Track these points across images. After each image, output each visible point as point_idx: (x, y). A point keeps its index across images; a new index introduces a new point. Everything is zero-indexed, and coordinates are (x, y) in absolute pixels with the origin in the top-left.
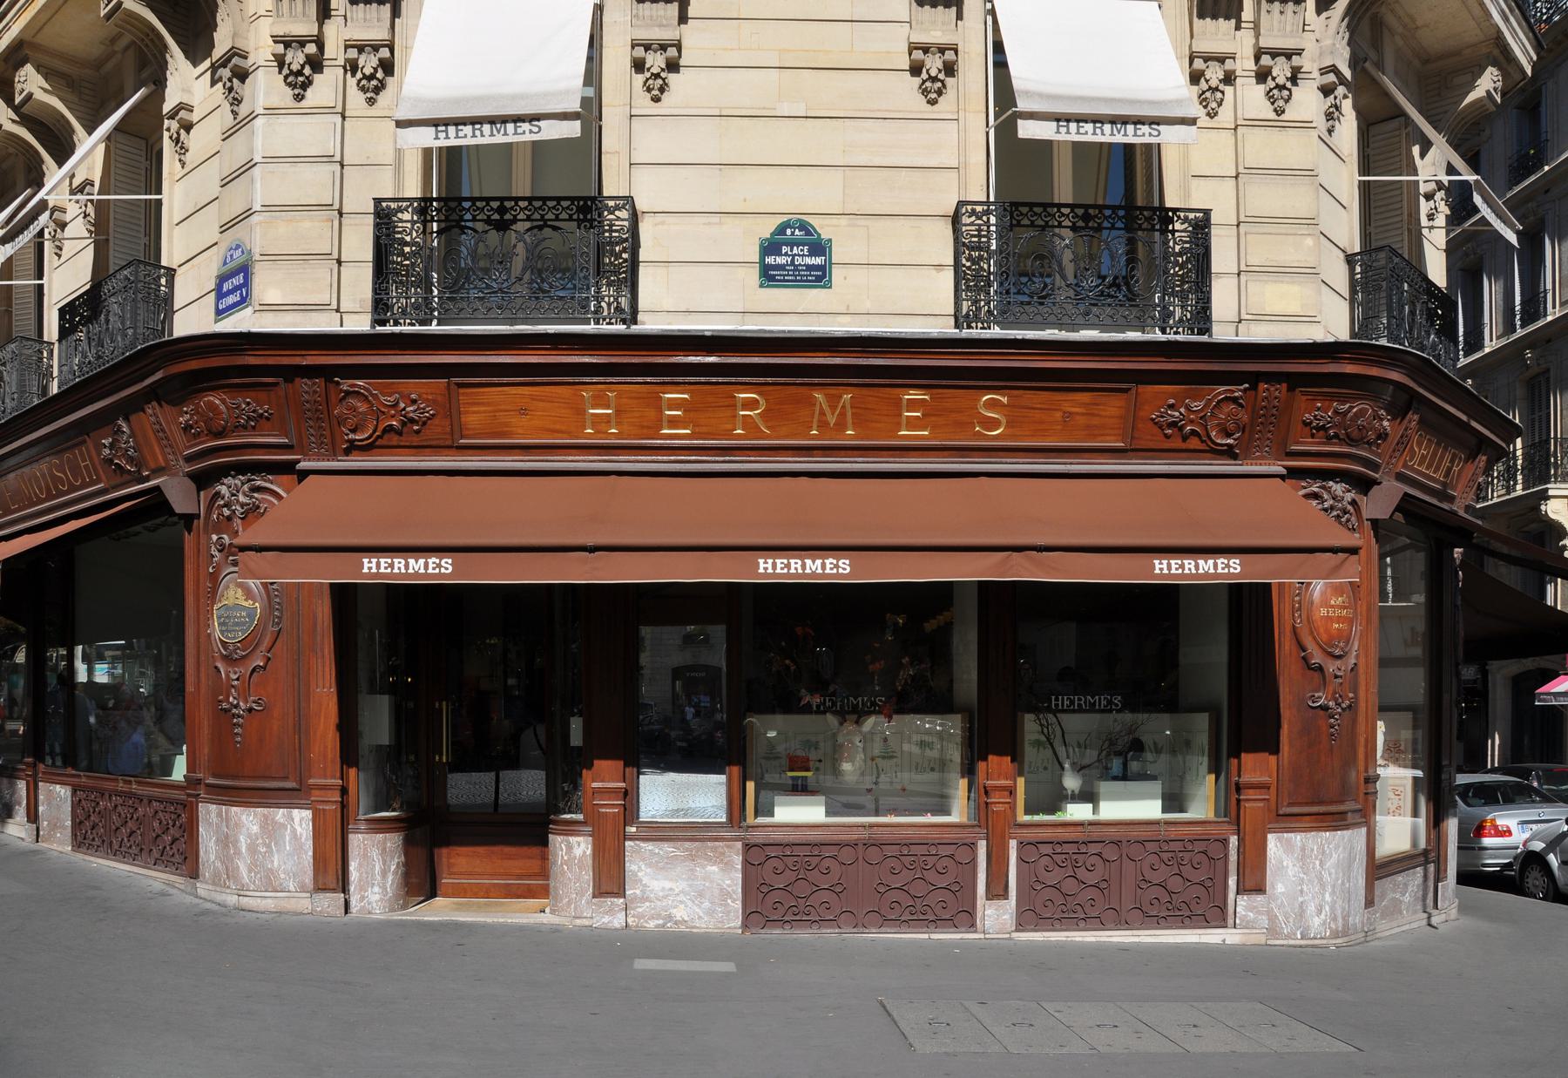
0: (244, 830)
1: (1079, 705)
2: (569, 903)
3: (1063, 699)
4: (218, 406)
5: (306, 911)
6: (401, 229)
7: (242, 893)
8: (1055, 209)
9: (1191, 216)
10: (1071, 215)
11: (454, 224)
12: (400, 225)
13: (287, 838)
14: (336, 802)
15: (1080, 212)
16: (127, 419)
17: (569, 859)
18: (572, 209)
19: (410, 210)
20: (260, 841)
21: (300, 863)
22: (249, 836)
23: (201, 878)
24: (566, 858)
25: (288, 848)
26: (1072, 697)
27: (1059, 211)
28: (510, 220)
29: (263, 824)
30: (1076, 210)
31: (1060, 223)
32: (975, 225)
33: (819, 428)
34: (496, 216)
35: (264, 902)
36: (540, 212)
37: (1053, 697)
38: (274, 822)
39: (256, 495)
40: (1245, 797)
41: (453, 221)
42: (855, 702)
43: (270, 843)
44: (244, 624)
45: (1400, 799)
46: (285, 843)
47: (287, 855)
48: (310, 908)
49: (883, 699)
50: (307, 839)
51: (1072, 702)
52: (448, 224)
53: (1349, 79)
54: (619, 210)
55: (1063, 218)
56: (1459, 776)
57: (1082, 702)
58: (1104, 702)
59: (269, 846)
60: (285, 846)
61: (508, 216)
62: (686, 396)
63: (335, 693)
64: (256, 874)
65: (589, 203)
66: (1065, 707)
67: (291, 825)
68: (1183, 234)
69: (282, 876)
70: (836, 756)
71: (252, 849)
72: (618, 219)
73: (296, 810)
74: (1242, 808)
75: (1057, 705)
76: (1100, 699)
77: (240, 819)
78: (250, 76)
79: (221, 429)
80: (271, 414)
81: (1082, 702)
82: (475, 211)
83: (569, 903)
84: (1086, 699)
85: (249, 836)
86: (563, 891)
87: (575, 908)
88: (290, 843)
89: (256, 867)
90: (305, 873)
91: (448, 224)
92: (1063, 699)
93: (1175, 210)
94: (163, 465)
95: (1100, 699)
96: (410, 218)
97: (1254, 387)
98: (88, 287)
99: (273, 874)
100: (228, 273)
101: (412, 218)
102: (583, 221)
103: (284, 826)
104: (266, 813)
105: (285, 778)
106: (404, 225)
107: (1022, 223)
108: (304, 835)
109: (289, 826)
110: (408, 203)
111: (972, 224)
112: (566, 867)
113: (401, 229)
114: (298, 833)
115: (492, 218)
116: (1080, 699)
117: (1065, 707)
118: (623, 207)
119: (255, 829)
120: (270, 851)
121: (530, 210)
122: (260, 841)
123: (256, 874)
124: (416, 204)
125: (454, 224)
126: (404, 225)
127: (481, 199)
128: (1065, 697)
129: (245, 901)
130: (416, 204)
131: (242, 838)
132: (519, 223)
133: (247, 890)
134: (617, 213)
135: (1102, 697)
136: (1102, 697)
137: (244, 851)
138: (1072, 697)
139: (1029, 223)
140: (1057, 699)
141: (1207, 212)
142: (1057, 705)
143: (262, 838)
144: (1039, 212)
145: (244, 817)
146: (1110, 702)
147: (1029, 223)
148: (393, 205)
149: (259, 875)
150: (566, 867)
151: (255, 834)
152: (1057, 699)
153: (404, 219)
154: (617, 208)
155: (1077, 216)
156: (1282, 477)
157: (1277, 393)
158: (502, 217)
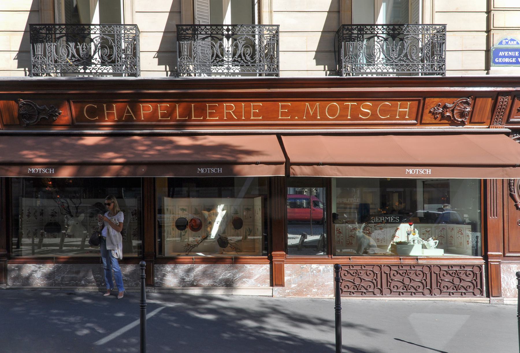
6: (41, 37)
8: (375, 27)
9: (438, 27)
10: (387, 29)
11: (64, 35)
12: (41, 35)
15: (391, 27)
18: (95, 30)
19: (191, 29)
27: (377, 27)
28: (396, 34)
30: (390, 27)
31: (366, 32)
32: (349, 34)
33: (399, 116)
34: (391, 32)
36: (88, 30)
40: (275, 260)
41: (63, 33)
45: (429, 234)
49: (398, 217)
51: (379, 219)
52: (61, 35)
54: (188, 30)
55: (218, 31)
58: (392, 219)
61: (396, 32)
62: (390, 104)
65: (362, 27)
66: (391, 221)
68: (347, 35)
70: (196, 243)
72: (187, 34)
74: (274, 264)
76: (390, 218)
82: (61, 30)
84: (385, 218)
91: (61, 35)
93: (200, 26)
95: (390, 218)
96: (357, 33)
97: (475, 99)
101: (358, 32)
102: (48, 34)
106: (43, 35)
107: (368, 33)
110: (44, 26)
111: (347, 34)
113: (41, 37)
115: (390, 32)
117: (391, 221)
118: (190, 29)
121: (399, 30)
124: (359, 27)
125: (64, 35)
126: (43, 35)
127: (397, 25)
130: (359, 27)
132: (401, 35)
134: (187, 31)
135: (391, 217)
136: (391, 217)
139: (370, 33)
141: (444, 26)
144: (380, 28)
146: (395, 219)
147: (370, 33)
148: (38, 27)
153: (189, 33)
154: (187, 29)
155: (390, 29)
156: (508, 134)
157: (506, 100)
158: (228, 33)
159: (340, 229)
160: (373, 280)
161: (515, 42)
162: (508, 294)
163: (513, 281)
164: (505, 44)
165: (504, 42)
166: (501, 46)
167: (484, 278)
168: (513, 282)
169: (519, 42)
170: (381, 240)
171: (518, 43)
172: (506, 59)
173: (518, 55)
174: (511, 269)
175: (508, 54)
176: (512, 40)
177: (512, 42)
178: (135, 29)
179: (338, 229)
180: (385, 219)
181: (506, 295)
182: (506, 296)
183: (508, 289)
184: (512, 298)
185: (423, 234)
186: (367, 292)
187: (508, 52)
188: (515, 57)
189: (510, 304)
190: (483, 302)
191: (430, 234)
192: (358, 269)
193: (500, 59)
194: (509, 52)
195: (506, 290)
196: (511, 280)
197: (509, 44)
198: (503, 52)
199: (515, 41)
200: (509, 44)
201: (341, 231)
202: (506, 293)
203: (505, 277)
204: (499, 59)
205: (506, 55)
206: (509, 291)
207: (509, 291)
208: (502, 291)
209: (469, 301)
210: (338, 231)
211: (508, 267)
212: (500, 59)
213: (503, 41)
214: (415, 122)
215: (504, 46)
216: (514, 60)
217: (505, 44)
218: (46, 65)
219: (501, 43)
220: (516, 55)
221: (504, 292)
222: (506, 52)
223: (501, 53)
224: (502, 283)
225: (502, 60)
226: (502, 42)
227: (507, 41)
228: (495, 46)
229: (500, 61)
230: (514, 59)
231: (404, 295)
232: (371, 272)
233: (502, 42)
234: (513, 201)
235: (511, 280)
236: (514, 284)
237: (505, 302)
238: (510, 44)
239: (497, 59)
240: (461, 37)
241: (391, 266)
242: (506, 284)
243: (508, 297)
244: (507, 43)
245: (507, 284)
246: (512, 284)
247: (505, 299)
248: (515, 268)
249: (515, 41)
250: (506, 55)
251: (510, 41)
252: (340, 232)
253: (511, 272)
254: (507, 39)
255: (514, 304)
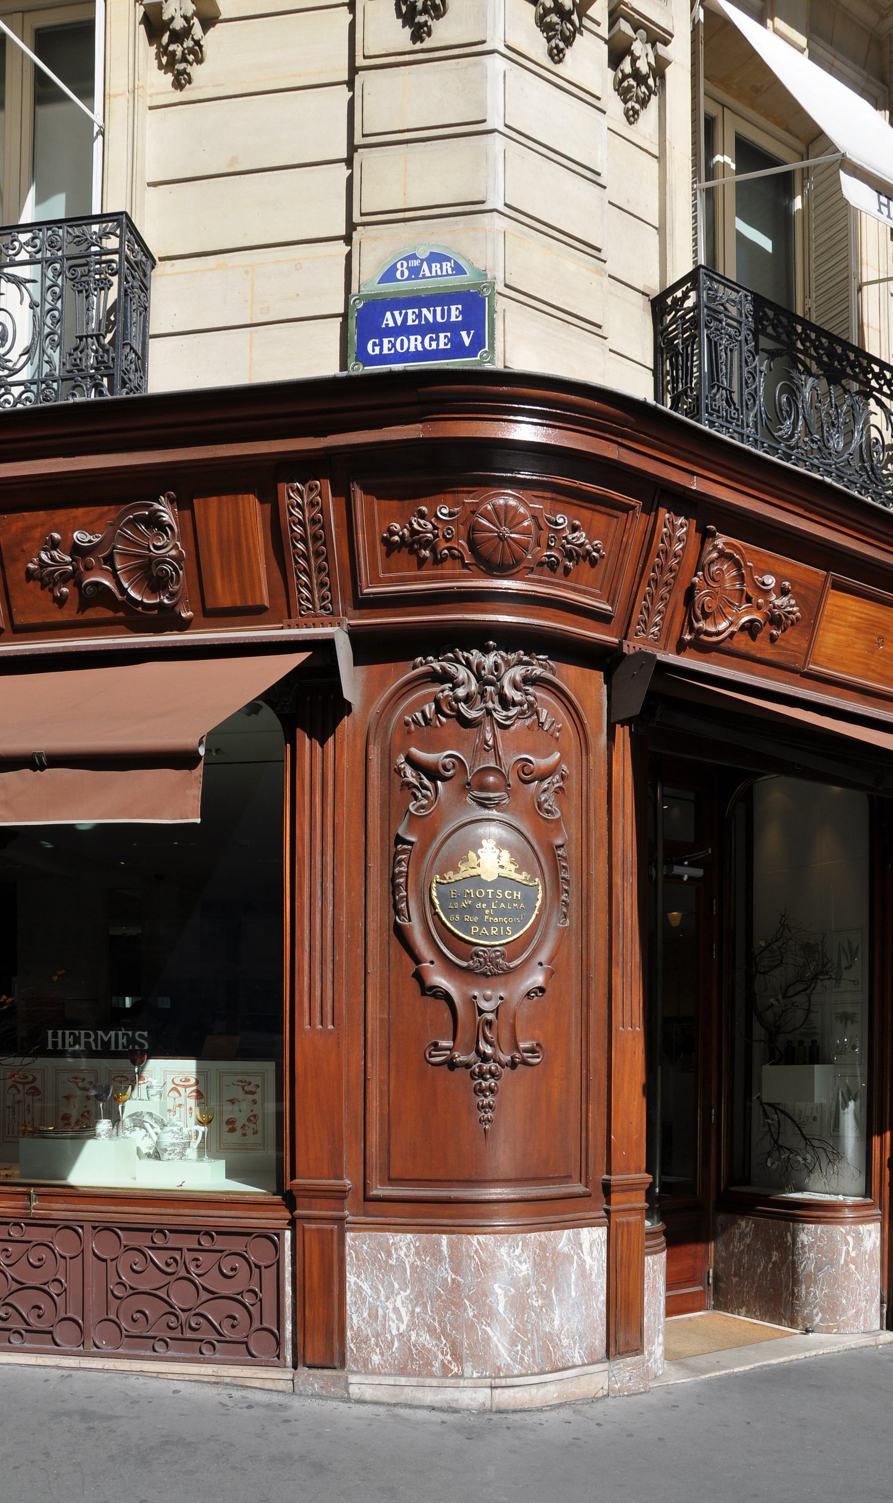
0: (503, 1274)
1: (88, 1044)
2: (858, 1315)
3: (63, 1034)
4: (515, 508)
5: (600, 1394)
7: (498, 1382)
13: (573, 1277)
14: (641, 1209)
16: (182, 503)
17: (858, 1255)
20: (533, 1288)
21: (588, 1316)
22: (514, 1282)
23: (350, 1364)
24: (853, 1254)
25: (573, 1294)
26: (77, 1032)
29: (538, 1259)
35: (543, 1390)
37: (50, 1032)
38: (556, 1254)
39: (531, 690)
42: (106, 1039)
43: (549, 1290)
44: (516, 912)
45: (254, 1101)
46: (569, 1286)
47: (573, 1306)
48: (606, 1387)
49: (145, 1034)
50: (598, 1276)
51: (77, 1041)
53: (311, 653)
56: (817, 1099)
57: (91, 1040)
59: (546, 1295)
60: (570, 1292)
63: (642, 1033)
64: (525, 1345)
66: (120, 1048)
67: (578, 1254)
69: (565, 1342)
71: (519, 1304)
73: (585, 1229)
75: (55, 1044)
76: (117, 1036)
77: (493, 1255)
78: (218, 25)
79: (498, 558)
80: (602, 557)
81: (91, 1040)
83: (858, 1315)
84: (96, 1035)
85: (514, 1282)
86: (847, 1299)
87: (865, 1320)
88: (576, 1285)
89: (525, 1334)
90: (595, 1330)
92: (63, 1034)
94: (266, 603)
95: (117, 1036)
98: (779, 23)
99: (551, 1341)
100: (389, 298)
103: (568, 1258)
104: (543, 1239)
105: (567, 1178)
108: (595, 1268)
109: (575, 1257)
112: (853, 1267)
114: (588, 1267)
116: (87, 1036)
117: (120, 1048)
119: (525, 1269)
120: (549, 1305)
122: (533, 1288)
123: (525, 1345)
128: (67, 1032)
129: (506, 1397)
131: (498, 1290)
133: (506, 1377)
135: (120, 1033)
136: (67, 1032)
137: (501, 1309)
138: (77, 1032)
140: (55, 1035)
142: (55, 1044)
143: (537, 1283)
145: (503, 1251)
149: (530, 1348)
150: (853, 1267)
151: (524, 1277)
152: (55, 1035)
159: (34, 1080)
160: (246, 1295)
161: (447, 266)
162: (376, 1359)
163: (399, 1304)
164: (409, 279)
165: (402, 270)
166: (390, 288)
167: (288, 1289)
168: (396, 1310)
169: (462, 263)
170: (243, 1127)
171: (458, 270)
172: (412, 338)
173: (460, 319)
174: (389, 1255)
175: (419, 316)
176: (436, 258)
177: (435, 266)
178: (118, 232)
179: (30, 1078)
180: (96, 1040)
181: (366, 1361)
182: (365, 1366)
183: (377, 1336)
184: (390, 1375)
185: (232, 1101)
186: (27, 1331)
187: (416, 311)
188: (447, 326)
189: (375, 1399)
190: (269, 1385)
191: (259, 1102)
192: (185, 1246)
193: (385, 341)
194: (425, 311)
195: (366, 1340)
196: (387, 1298)
197: (424, 277)
198: (396, 313)
199: (448, 259)
200: (424, 277)
201: (37, 1084)
202: (364, 1354)
203: (365, 1286)
204: (381, 344)
205: (410, 323)
206: (377, 1345)
207: (377, 1345)
208: (351, 1345)
209: (213, 1379)
210: (27, 1087)
211: (379, 1244)
212: (385, 341)
213: (399, 266)
214: (598, 591)
215: (403, 286)
216: (443, 341)
217: (409, 279)
218: (111, 377)
219: (389, 276)
220: (453, 319)
221: (359, 1349)
222: (410, 312)
223: (388, 314)
224: (350, 1309)
225: (394, 345)
226: (394, 268)
227: (416, 263)
228: (365, 291)
229: (385, 351)
230: (442, 335)
231: (170, 1353)
232: (238, 1263)
233: (394, 268)
234: (406, 958)
235: (387, 1298)
236: (400, 1319)
237: (354, 1390)
238: (428, 274)
239: (374, 344)
240: (247, 272)
241: (121, 1229)
242: (365, 1315)
243: (373, 1373)
244: (415, 272)
245: (374, 1316)
246: (393, 1316)
247: (353, 1379)
248: (408, 1248)
249: (448, 259)
250: (410, 323)
251: (425, 265)
252: (34, 1088)
253: (391, 1266)
254: (414, 257)
255: (393, 1402)
